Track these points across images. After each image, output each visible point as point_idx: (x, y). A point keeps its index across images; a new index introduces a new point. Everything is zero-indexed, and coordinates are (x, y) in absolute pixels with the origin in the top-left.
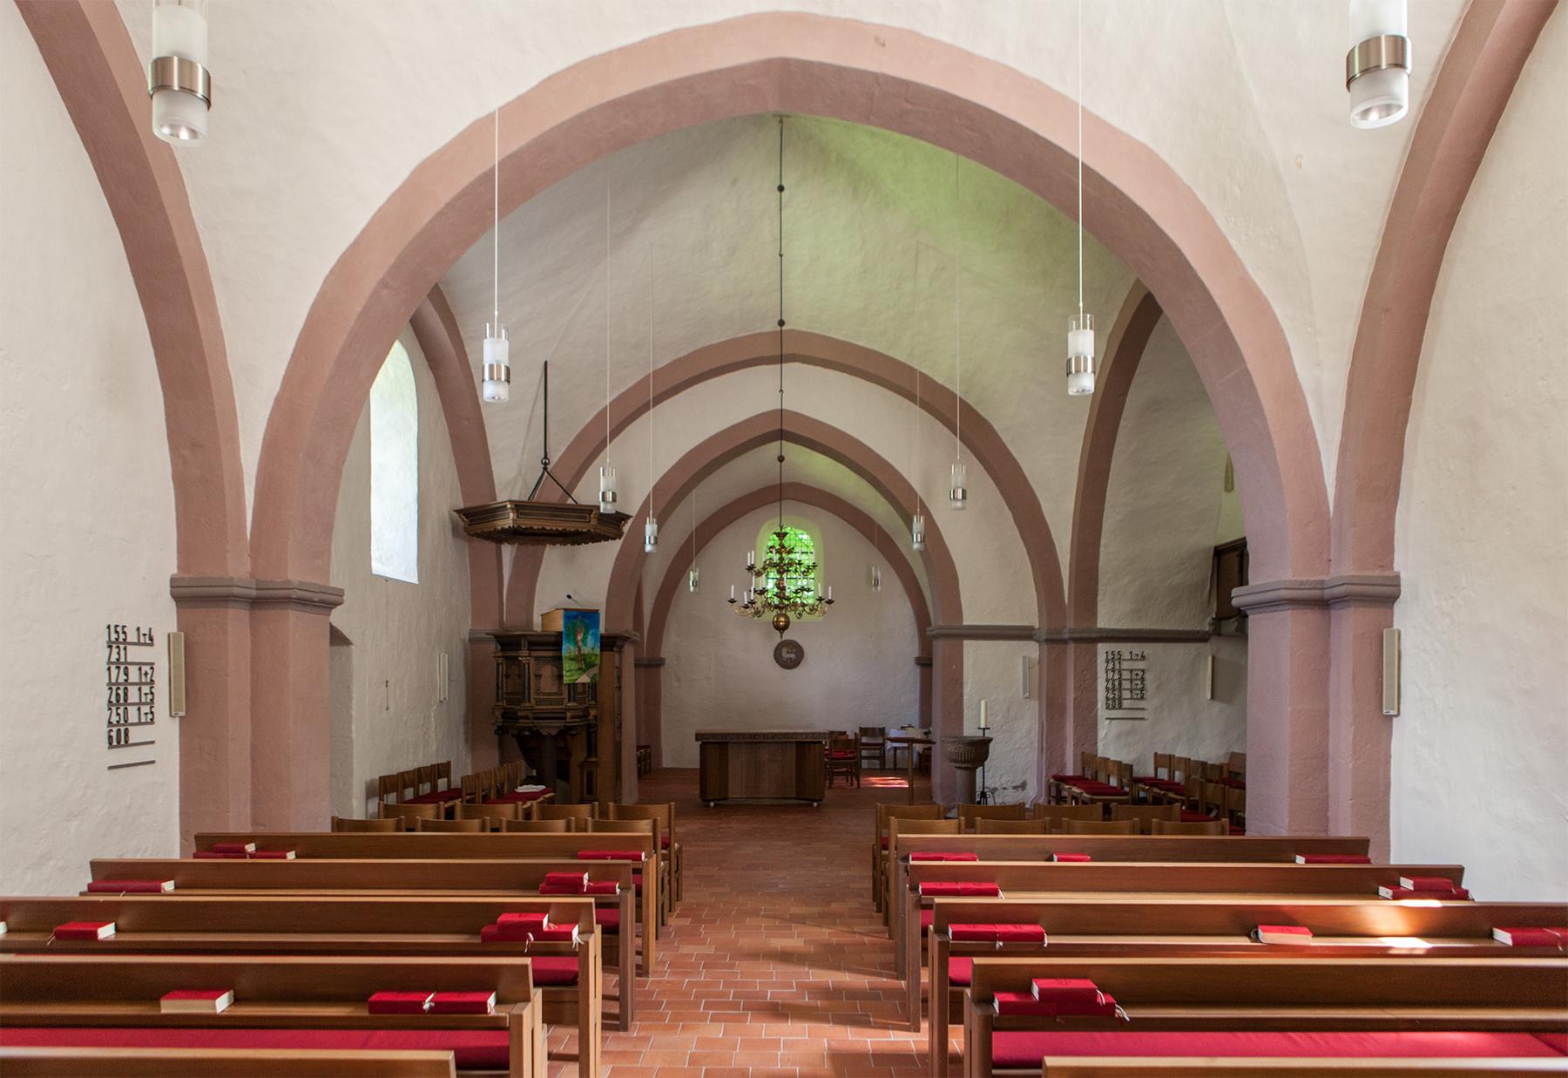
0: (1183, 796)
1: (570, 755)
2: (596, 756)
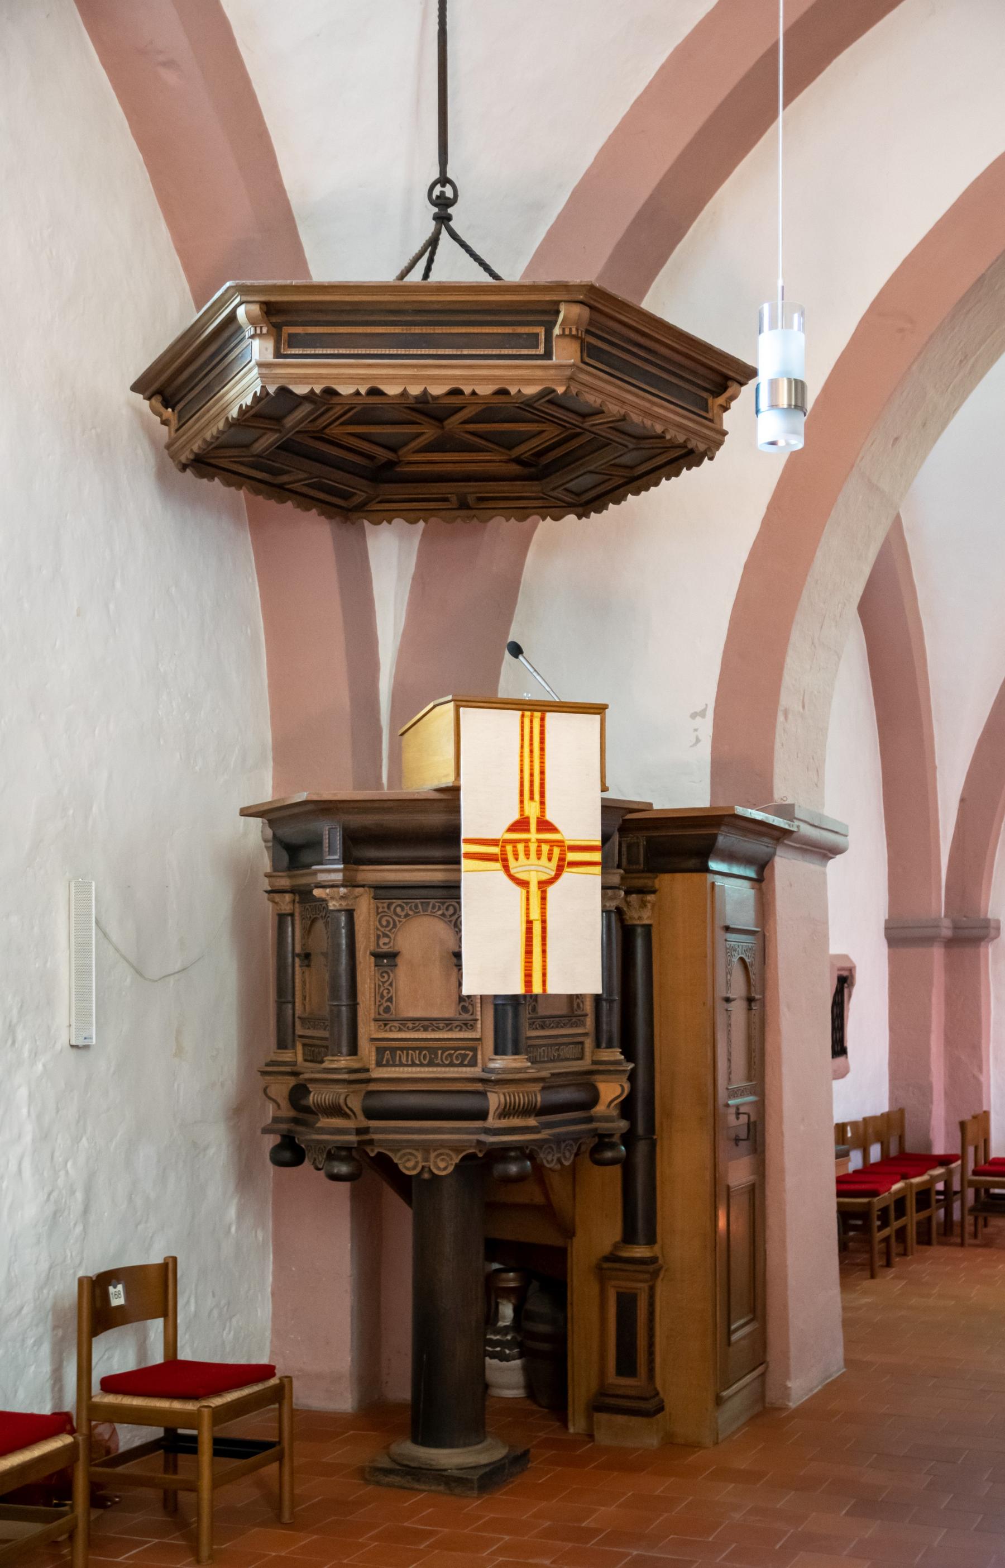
0: (388, 789)
1: (569, 1233)
2: (651, 1240)
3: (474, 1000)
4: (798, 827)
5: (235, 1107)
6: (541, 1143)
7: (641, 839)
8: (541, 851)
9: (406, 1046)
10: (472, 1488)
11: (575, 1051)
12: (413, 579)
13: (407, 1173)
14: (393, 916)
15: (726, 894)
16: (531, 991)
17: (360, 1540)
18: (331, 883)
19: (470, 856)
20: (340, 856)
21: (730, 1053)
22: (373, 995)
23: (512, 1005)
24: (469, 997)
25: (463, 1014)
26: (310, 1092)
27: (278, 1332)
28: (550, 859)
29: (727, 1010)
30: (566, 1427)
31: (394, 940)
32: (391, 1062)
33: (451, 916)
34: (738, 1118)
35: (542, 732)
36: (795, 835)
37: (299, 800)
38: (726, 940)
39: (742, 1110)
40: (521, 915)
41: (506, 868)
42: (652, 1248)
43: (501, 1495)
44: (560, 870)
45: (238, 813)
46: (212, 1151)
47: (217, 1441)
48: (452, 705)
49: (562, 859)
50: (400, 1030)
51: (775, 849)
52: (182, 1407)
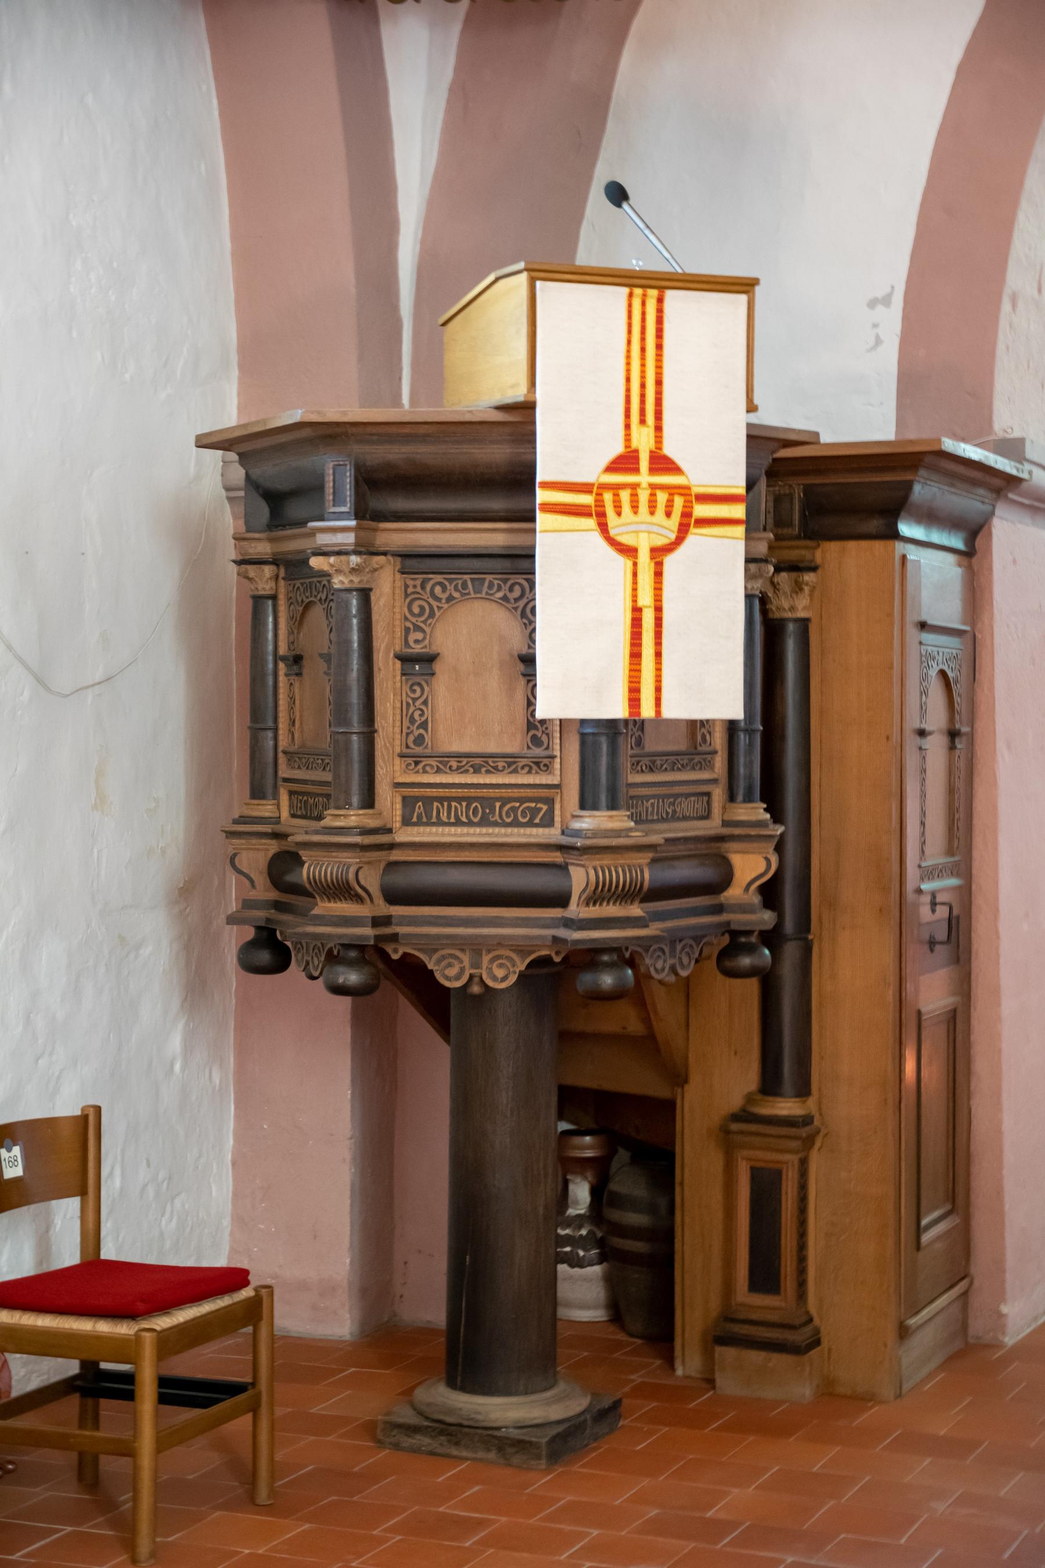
1: (679, 1078)
2: (803, 1091)
3: (550, 728)
4: (1030, 473)
5: (181, 885)
6: (646, 943)
7: (796, 487)
8: (655, 501)
9: (448, 795)
10: (538, 1457)
11: (700, 805)
12: (451, 90)
13: (447, 984)
14: (431, 600)
15: (923, 574)
16: (639, 714)
17: (375, 1532)
18: (336, 549)
19: (551, 508)
20: (350, 508)
21: (923, 813)
22: (398, 717)
23: (607, 735)
24: (543, 722)
25: (533, 748)
26: (303, 863)
27: (239, 1220)
28: (668, 514)
29: (920, 748)
30: (672, 1367)
31: (430, 636)
32: (425, 820)
33: (516, 600)
34: (933, 911)
35: (660, 321)
36: (1024, 485)
37: (290, 422)
38: (921, 643)
39: (939, 899)
40: (625, 599)
41: (603, 528)
42: (804, 1102)
43: (582, 1466)
44: (683, 531)
45: (193, 444)
46: (147, 951)
47: (163, 1382)
48: (524, 277)
49: (686, 514)
50: (439, 771)
51: (994, 507)
52: (110, 1330)
